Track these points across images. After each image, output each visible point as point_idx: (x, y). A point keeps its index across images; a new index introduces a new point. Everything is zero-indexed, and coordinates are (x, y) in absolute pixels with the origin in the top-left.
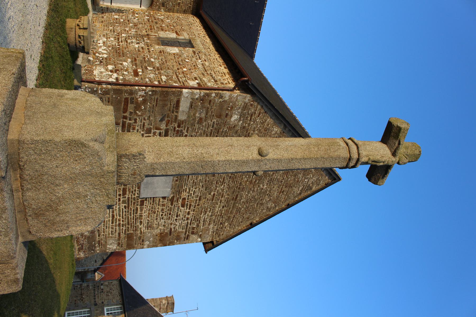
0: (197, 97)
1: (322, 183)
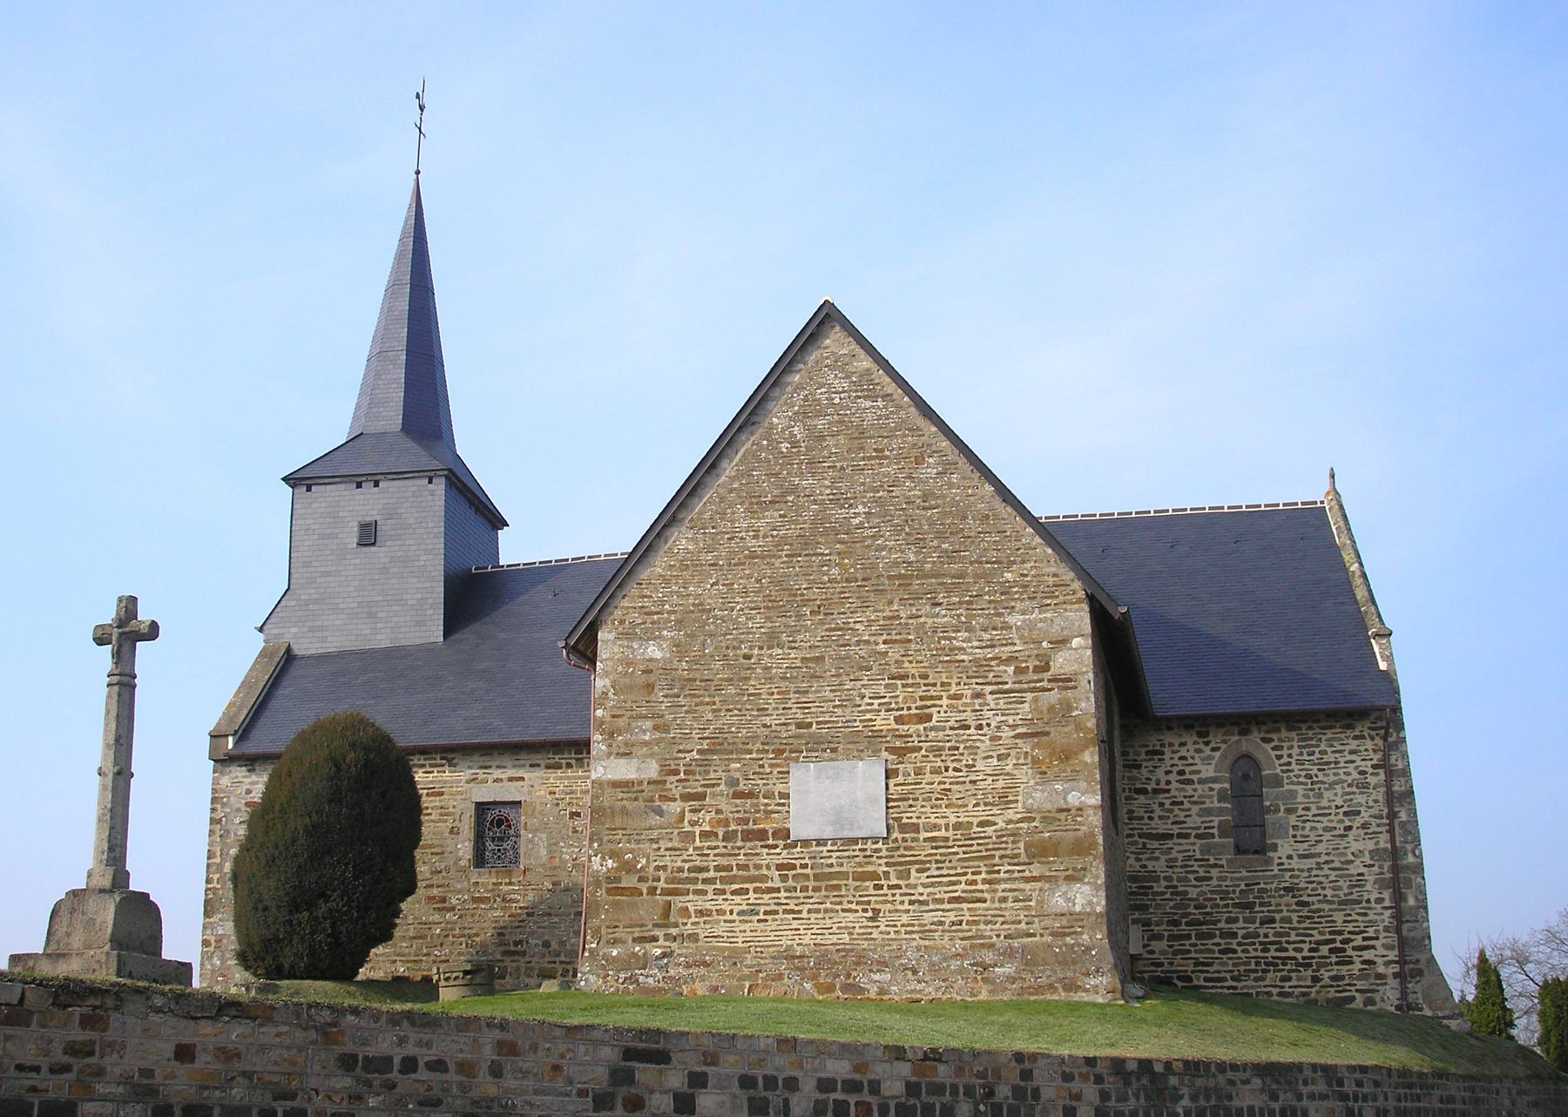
0: (604, 748)
1: (849, 347)
